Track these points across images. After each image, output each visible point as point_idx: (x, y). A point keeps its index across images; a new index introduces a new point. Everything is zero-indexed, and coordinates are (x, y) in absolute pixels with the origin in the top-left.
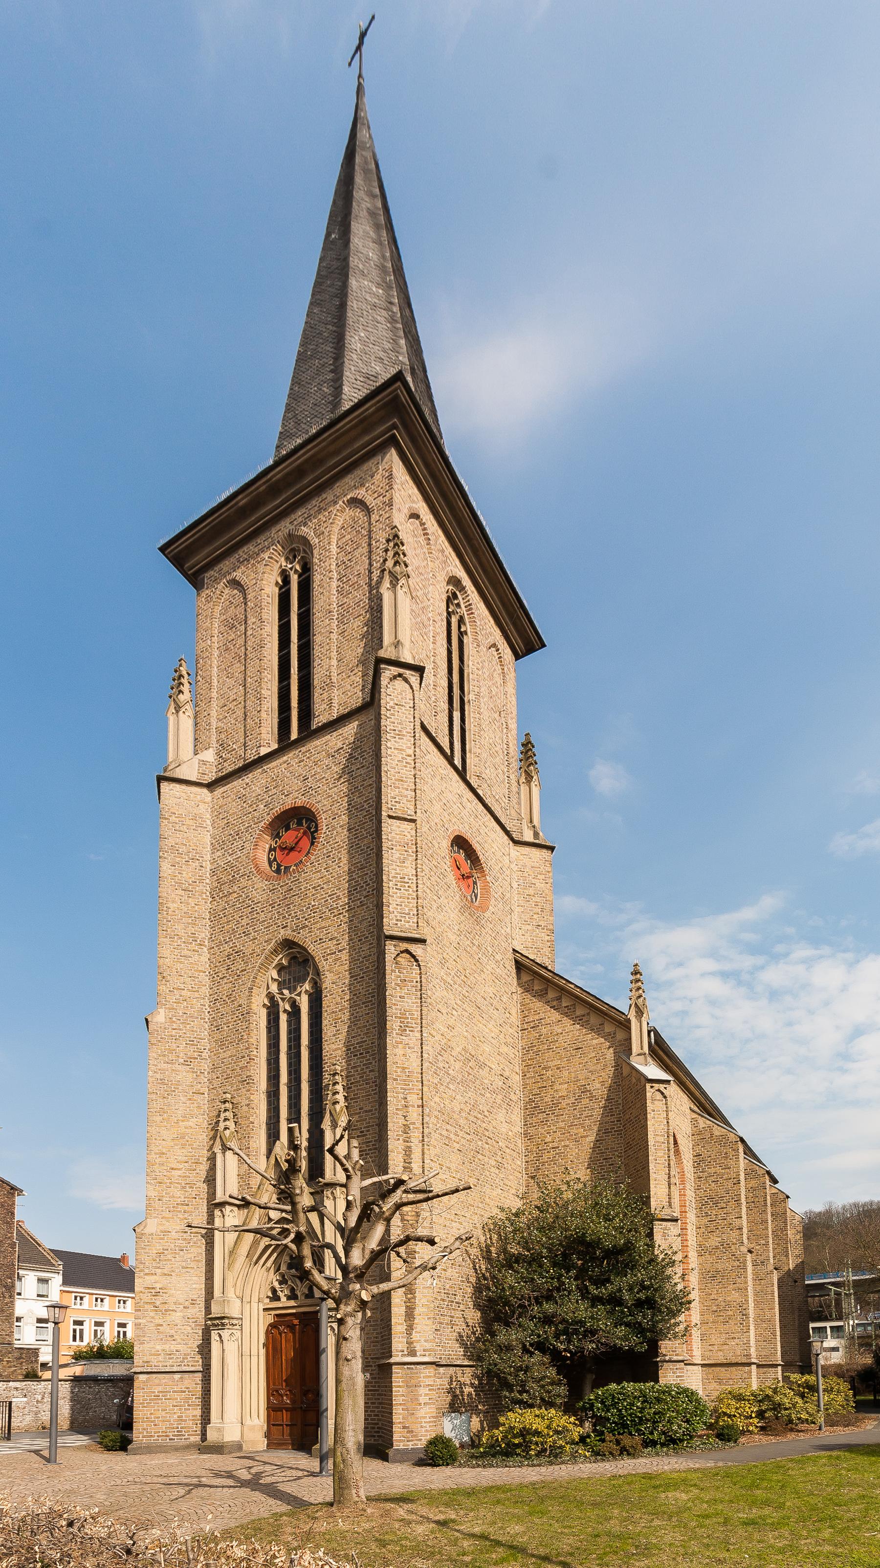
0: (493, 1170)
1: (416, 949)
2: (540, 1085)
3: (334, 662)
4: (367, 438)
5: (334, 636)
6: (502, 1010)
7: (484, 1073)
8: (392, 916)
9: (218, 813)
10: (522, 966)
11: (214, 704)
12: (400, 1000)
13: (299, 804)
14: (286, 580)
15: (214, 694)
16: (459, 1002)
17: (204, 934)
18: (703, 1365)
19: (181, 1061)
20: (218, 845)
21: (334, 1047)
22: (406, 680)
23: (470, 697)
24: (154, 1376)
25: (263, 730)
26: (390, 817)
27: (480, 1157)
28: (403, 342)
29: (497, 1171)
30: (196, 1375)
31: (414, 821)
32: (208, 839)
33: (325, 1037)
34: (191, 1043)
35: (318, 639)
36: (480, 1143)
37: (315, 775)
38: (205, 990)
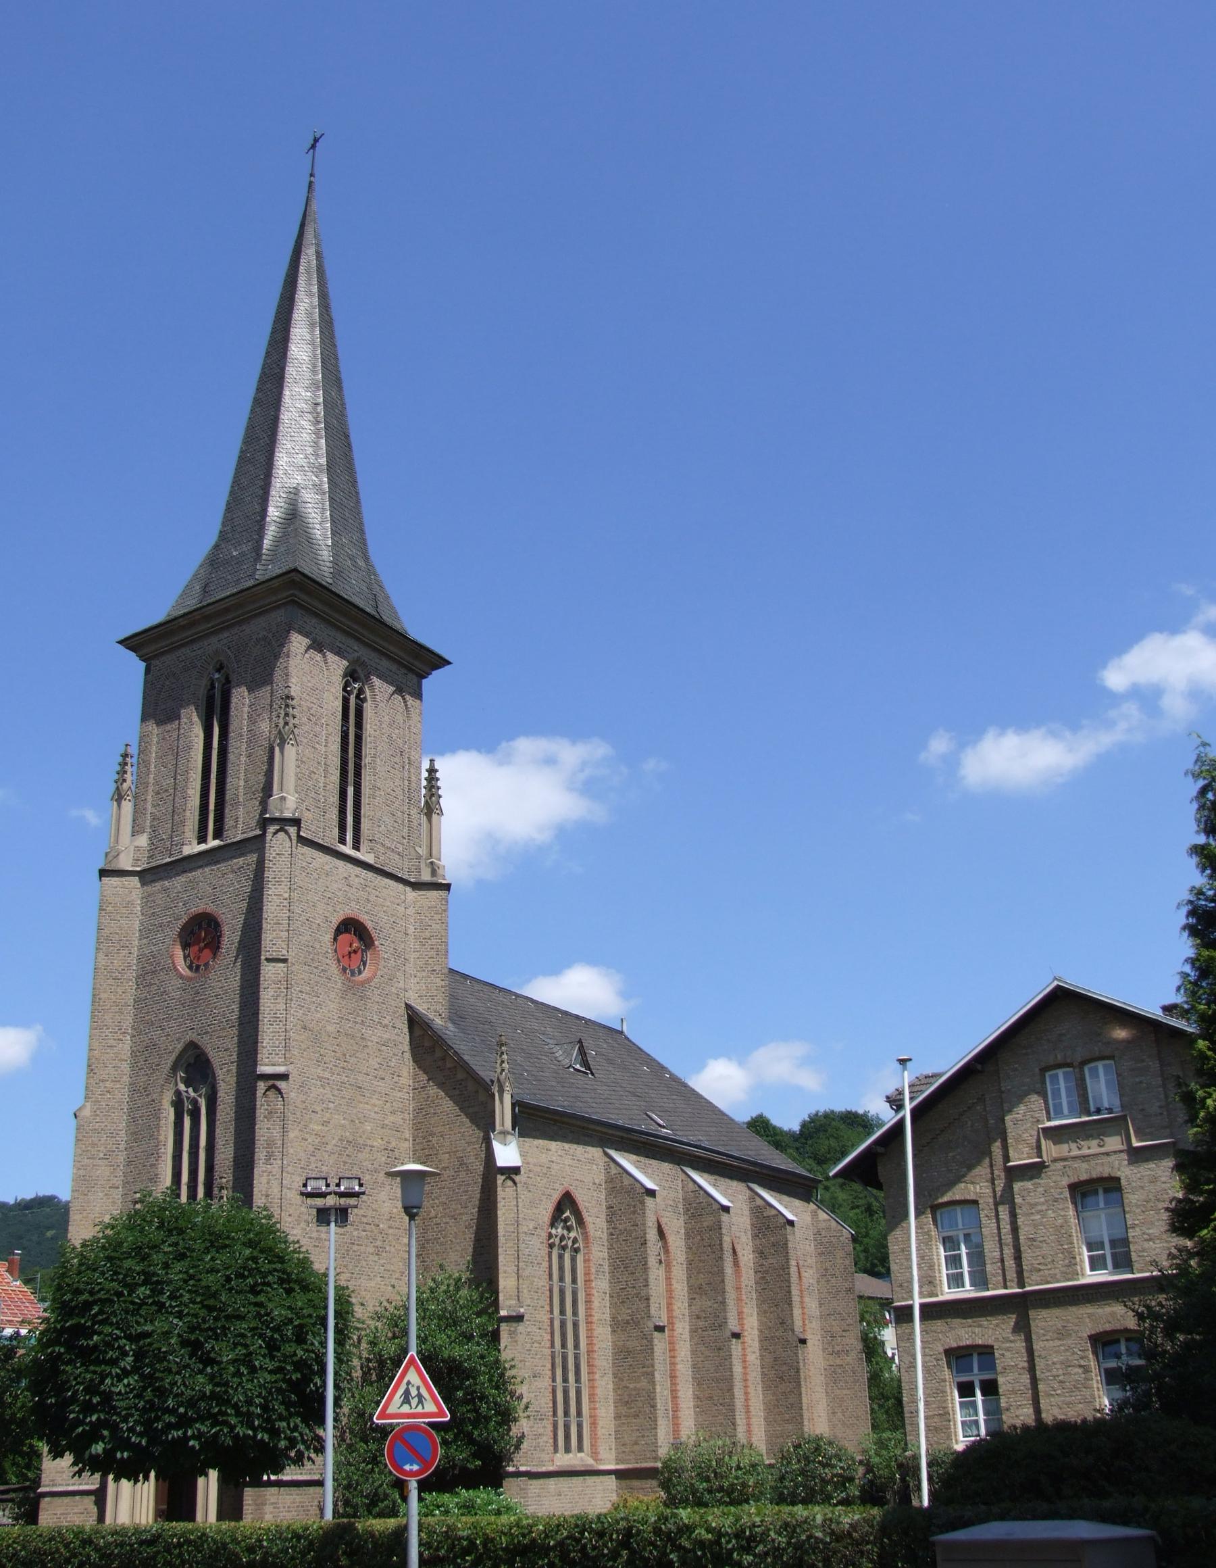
0: (371, 1257)
1: (282, 1085)
2: (426, 1151)
3: (242, 783)
4: (274, 598)
5: (243, 759)
6: (388, 1077)
7: (364, 1155)
8: (265, 1051)
9: (147, 900)
10: (415, 1021)
11: (151, 788)
12: (265, 1129)
13: (209, 910)
14: (213, 686)
15: (151, 780)
16: (336, 1092)
17: (128, 1022)
18: (620, 1475)
19: (101, 1155)
20: (145, 932)
21: (223, 1156)
22: (286, 832)
23: (366, 760)
24: (552, 1483)
25: (187, 829)
26: (268, 960)
27: (355, 1247)
28: (323, 441)
29: (376, 1258)
30: (1030, 1411)
31: (285, 961)
32: (137, 926)
33: (217, 1147)
34: (112, 1135)
35: (231, 757)
36: (355, 1233)
37: (219, 890)
38: (126, 1079)
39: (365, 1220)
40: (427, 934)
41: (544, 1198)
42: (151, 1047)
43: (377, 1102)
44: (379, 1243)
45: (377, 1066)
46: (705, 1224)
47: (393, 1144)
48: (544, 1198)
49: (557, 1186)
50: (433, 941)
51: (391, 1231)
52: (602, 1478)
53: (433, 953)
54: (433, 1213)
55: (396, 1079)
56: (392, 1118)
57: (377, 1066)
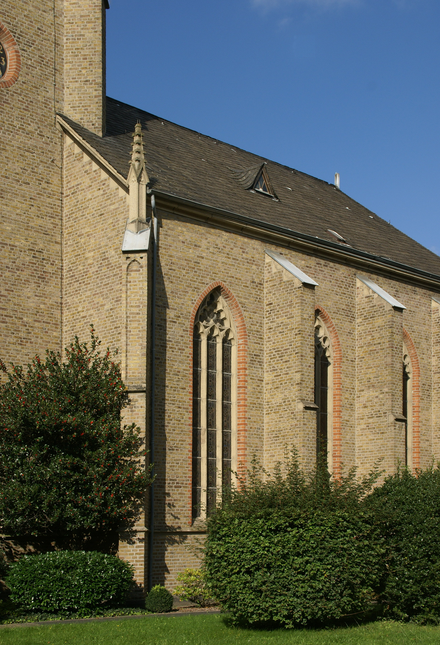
0: (12, 347)
29: (19, 347)
39: (5, 313)
40: (80, 44)
41: (190, 290)
42: (159, 283)
43: (19, 205)
44: (22, 335)
45: (19, 170)
46: (376, 325)
47: (41, 246)
48: (190, 290)
49: (207, 280)
50: (86, 52)
51: (37, 324)
52: (401, 384)
53: (86, 64)
54: (80, 309)
55: (44, 185)
56: (40, 222)
57: (19, 170)
